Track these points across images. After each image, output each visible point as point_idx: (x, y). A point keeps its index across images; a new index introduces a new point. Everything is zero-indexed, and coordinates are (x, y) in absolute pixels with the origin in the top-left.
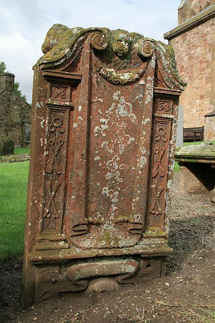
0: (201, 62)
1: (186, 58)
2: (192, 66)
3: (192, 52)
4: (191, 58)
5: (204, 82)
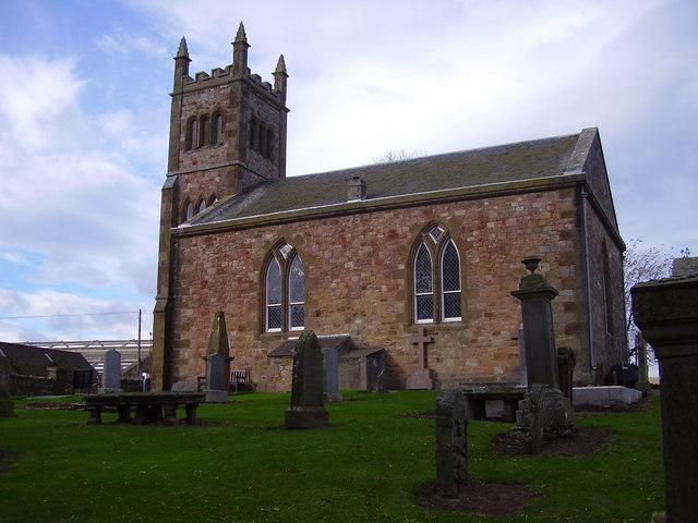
0: (240, 280)
1: (212, 271)
2: (224, 283)
3: (224, 264)
4: (221, 271)
5: (245, 308)
